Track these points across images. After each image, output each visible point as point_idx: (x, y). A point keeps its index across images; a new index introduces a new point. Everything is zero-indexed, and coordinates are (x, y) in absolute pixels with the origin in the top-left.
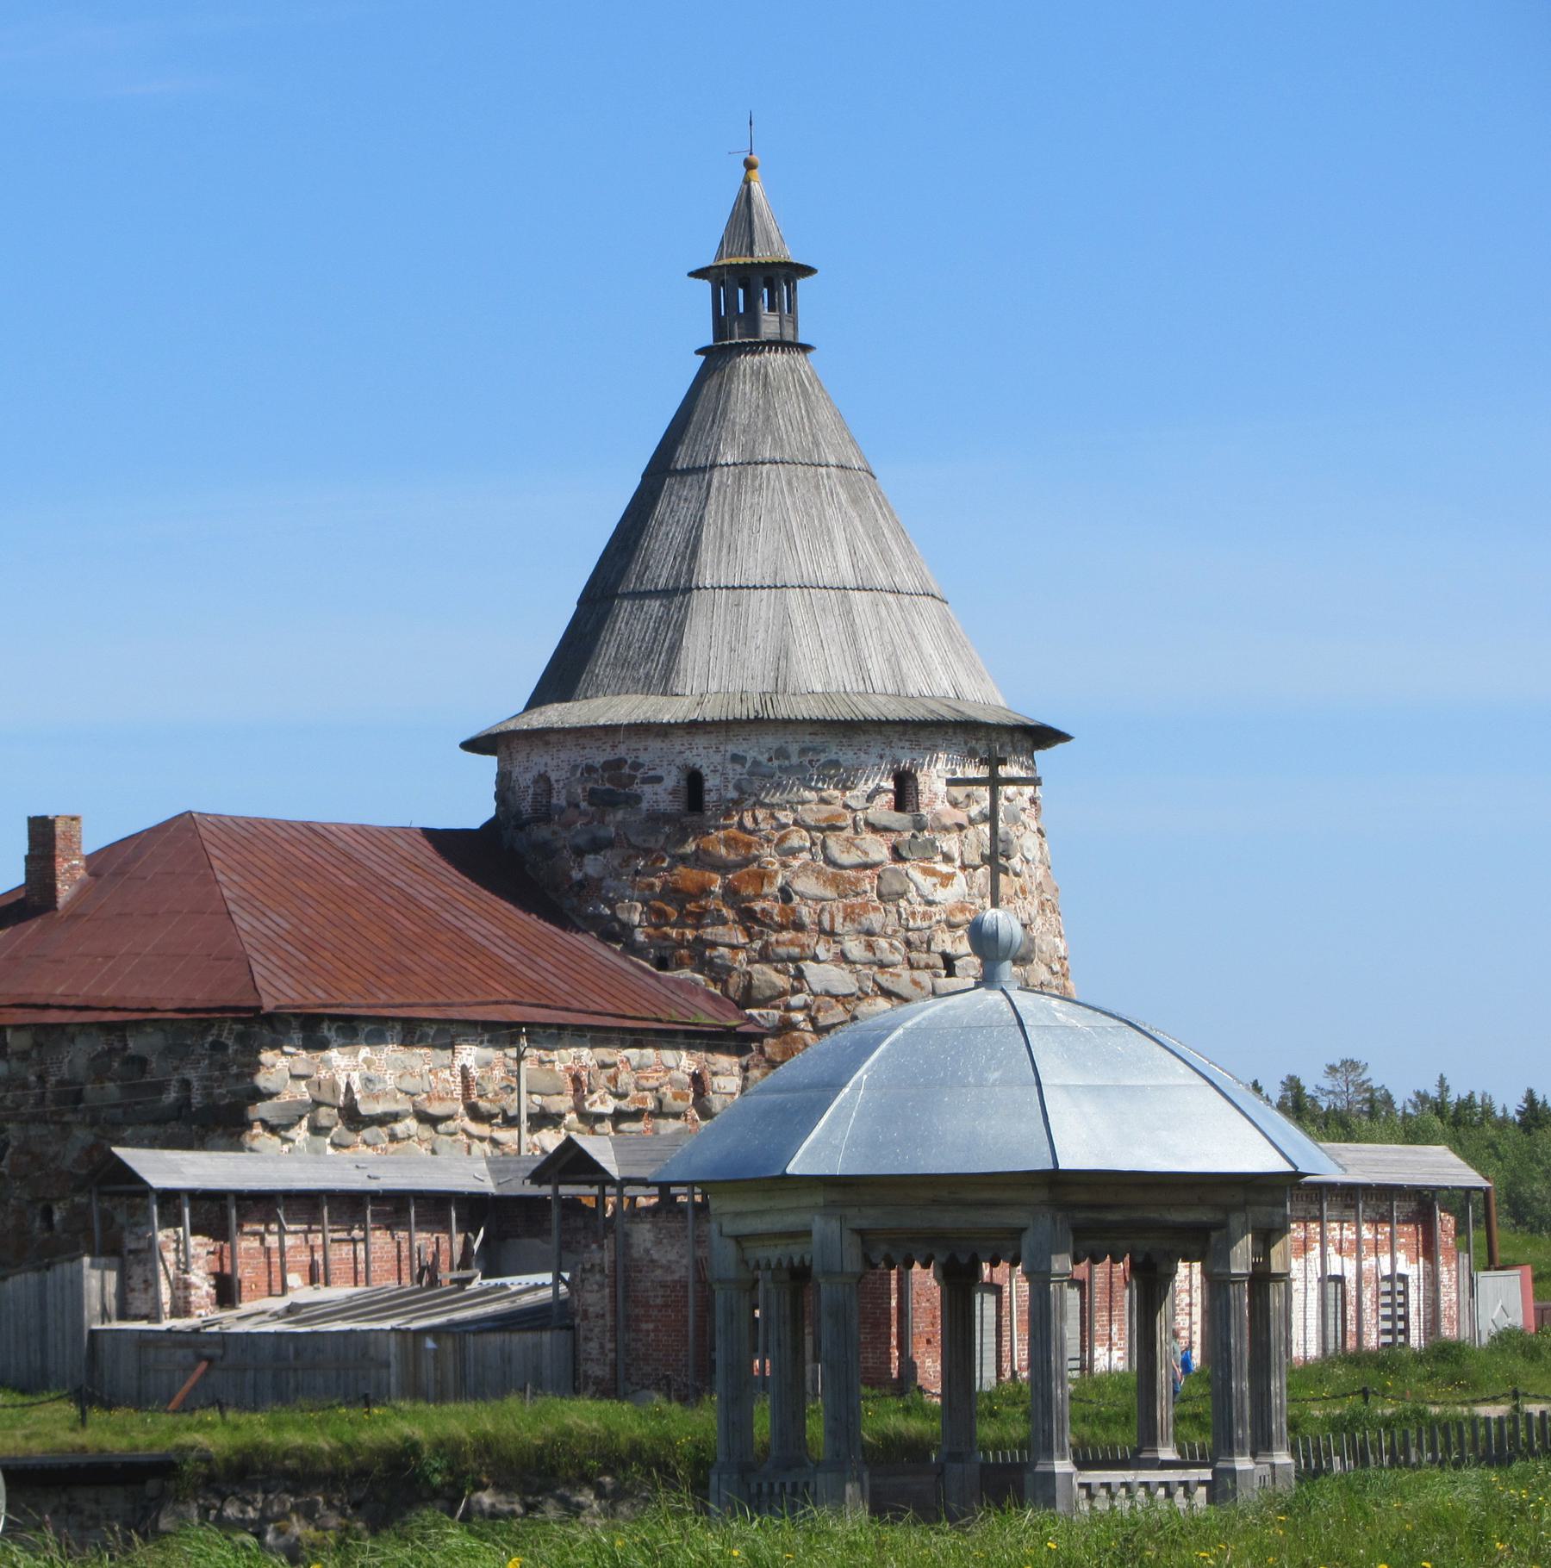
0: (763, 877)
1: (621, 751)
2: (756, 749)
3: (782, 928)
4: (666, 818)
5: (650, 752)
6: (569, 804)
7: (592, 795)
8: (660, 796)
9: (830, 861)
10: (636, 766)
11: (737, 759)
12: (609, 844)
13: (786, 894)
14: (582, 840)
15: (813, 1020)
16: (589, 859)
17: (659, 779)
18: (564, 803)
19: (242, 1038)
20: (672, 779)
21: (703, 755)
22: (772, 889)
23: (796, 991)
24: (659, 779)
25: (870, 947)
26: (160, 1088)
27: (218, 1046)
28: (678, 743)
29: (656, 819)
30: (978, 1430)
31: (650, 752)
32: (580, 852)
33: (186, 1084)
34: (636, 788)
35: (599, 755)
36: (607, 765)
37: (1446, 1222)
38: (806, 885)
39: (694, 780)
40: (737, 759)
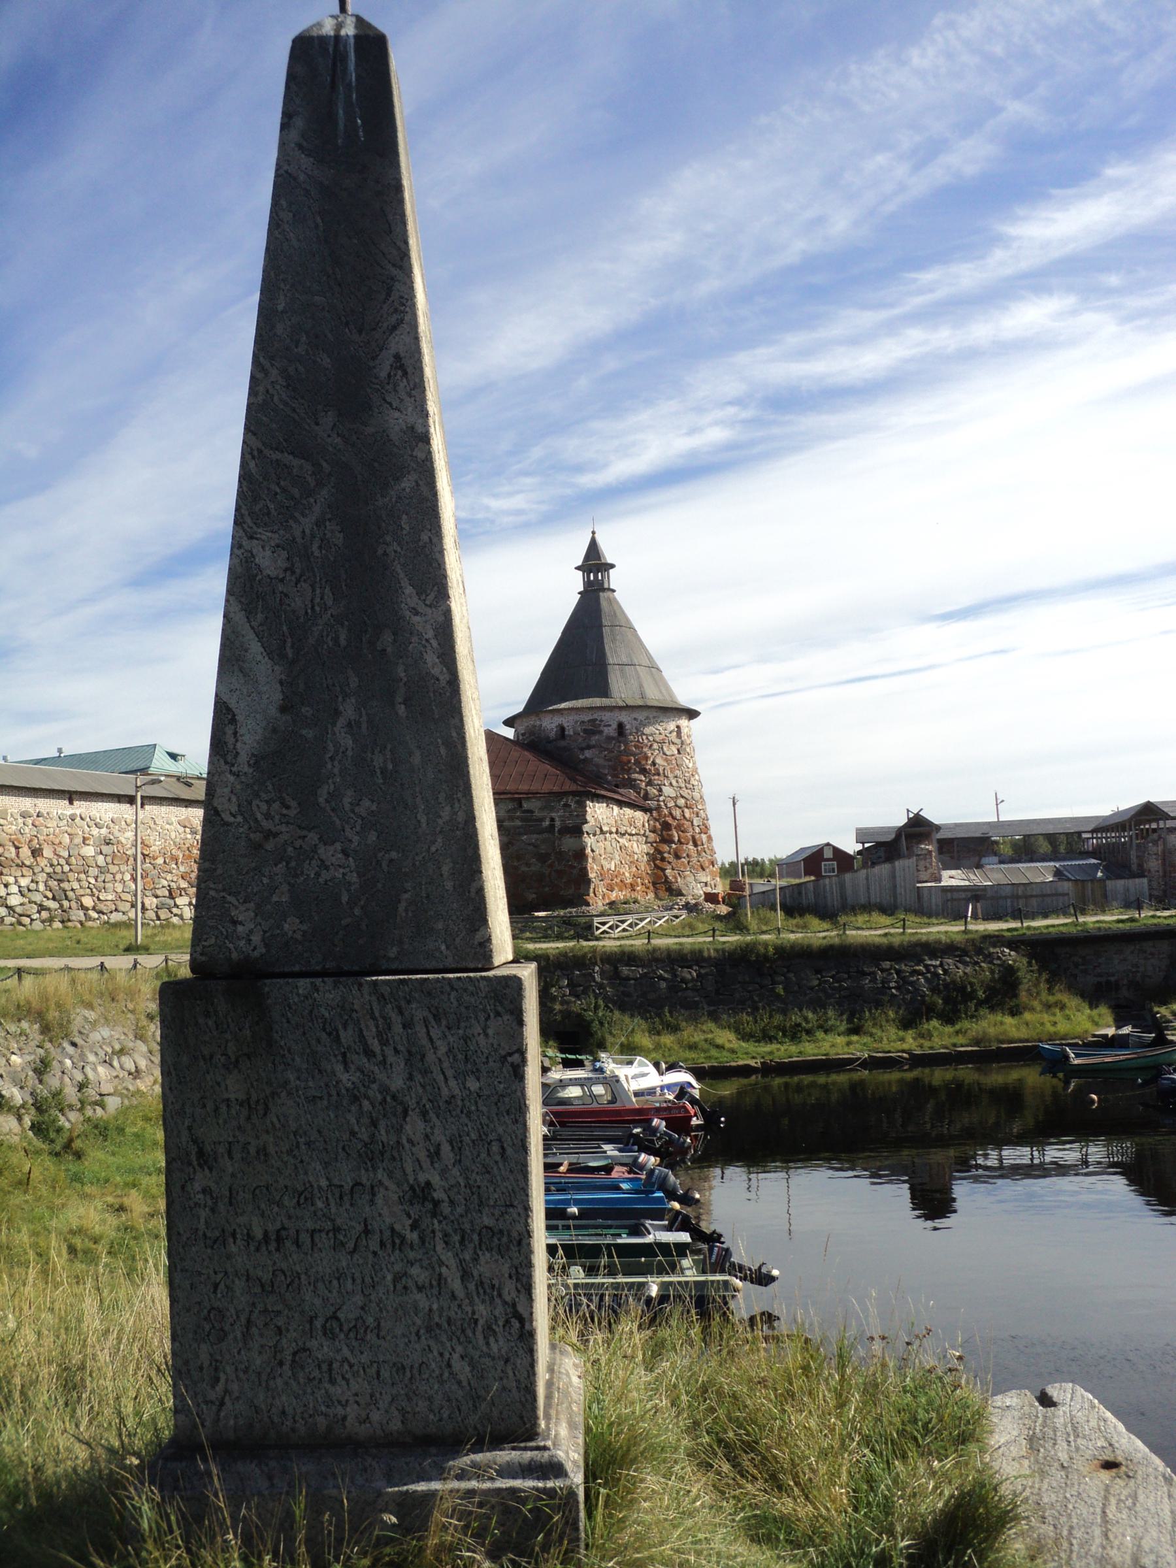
0: (647, 758)
1: (595, 716)
2: (642, 716)
3: (654, 775)
4: (613, 738)
5: (606, 716)
6: (575, 734)
7: (585, 731)
8: (611, 731)
9: (664, 754)
10: (601, 721)
11: (635, 719)
12: (594, 747)
13: (654, 764)
14: (584, 745)
15: (666, 805)
16: (586, 752)
17: (610, 725)
18: (572, 733)
19: (577, 802)
20: (615, 726)
21: (624, 717)
22: (650, 762)
23: (660, 796)
24: (610, 725)
25: (677, 782)
26: (542, 820)
27: (566, 805)
28: (616, 713)
29: (609, 739)
30: (184, 976)
31: (606, 716)
32: (582, 749)
33: (552, 820)
34: (601, 728)
35: (586, 717)
36: (589, 721)
37: (1134, 867)
38: (659, 761)
39: (621, 726)
40: (635, 719)
